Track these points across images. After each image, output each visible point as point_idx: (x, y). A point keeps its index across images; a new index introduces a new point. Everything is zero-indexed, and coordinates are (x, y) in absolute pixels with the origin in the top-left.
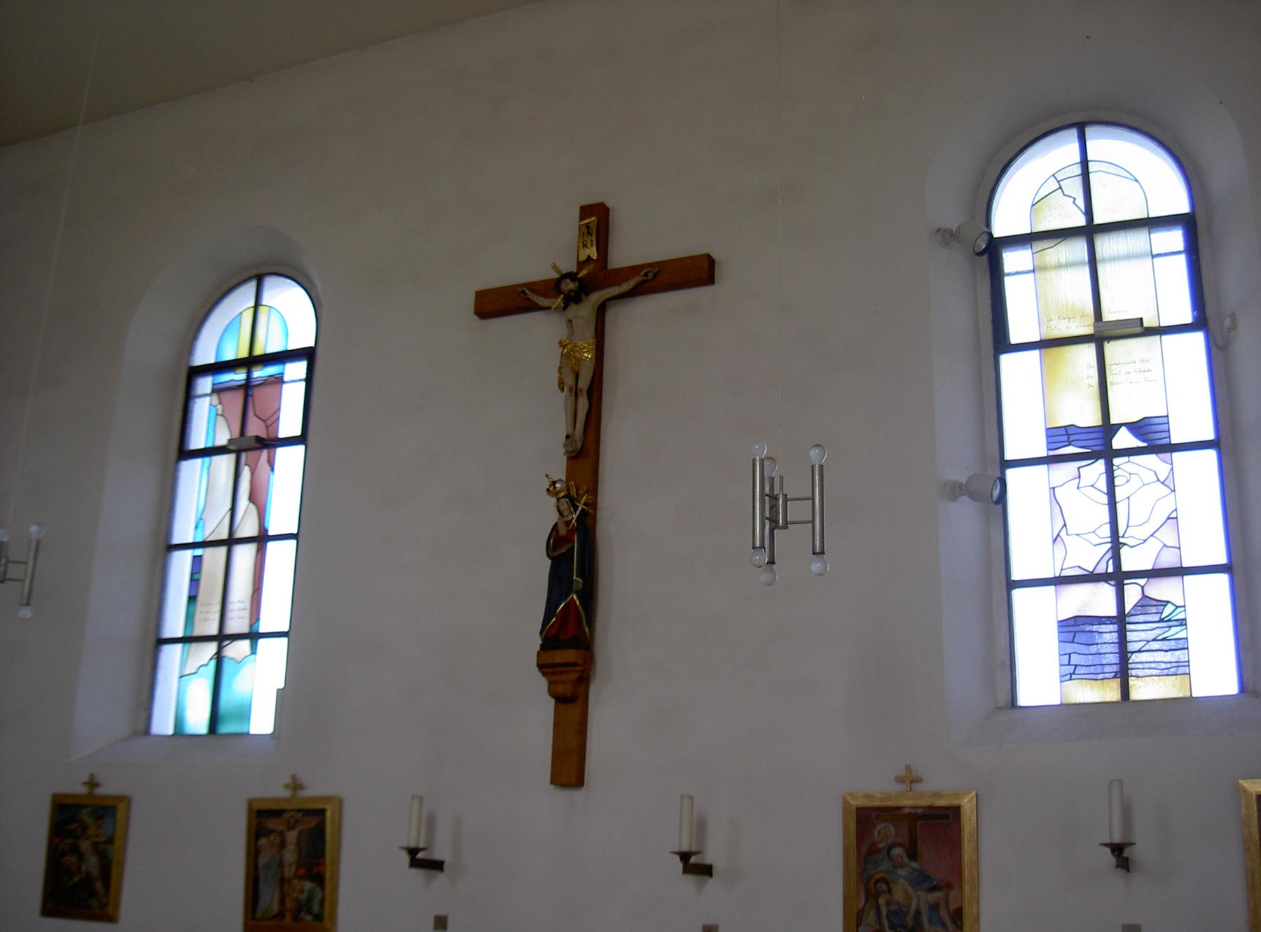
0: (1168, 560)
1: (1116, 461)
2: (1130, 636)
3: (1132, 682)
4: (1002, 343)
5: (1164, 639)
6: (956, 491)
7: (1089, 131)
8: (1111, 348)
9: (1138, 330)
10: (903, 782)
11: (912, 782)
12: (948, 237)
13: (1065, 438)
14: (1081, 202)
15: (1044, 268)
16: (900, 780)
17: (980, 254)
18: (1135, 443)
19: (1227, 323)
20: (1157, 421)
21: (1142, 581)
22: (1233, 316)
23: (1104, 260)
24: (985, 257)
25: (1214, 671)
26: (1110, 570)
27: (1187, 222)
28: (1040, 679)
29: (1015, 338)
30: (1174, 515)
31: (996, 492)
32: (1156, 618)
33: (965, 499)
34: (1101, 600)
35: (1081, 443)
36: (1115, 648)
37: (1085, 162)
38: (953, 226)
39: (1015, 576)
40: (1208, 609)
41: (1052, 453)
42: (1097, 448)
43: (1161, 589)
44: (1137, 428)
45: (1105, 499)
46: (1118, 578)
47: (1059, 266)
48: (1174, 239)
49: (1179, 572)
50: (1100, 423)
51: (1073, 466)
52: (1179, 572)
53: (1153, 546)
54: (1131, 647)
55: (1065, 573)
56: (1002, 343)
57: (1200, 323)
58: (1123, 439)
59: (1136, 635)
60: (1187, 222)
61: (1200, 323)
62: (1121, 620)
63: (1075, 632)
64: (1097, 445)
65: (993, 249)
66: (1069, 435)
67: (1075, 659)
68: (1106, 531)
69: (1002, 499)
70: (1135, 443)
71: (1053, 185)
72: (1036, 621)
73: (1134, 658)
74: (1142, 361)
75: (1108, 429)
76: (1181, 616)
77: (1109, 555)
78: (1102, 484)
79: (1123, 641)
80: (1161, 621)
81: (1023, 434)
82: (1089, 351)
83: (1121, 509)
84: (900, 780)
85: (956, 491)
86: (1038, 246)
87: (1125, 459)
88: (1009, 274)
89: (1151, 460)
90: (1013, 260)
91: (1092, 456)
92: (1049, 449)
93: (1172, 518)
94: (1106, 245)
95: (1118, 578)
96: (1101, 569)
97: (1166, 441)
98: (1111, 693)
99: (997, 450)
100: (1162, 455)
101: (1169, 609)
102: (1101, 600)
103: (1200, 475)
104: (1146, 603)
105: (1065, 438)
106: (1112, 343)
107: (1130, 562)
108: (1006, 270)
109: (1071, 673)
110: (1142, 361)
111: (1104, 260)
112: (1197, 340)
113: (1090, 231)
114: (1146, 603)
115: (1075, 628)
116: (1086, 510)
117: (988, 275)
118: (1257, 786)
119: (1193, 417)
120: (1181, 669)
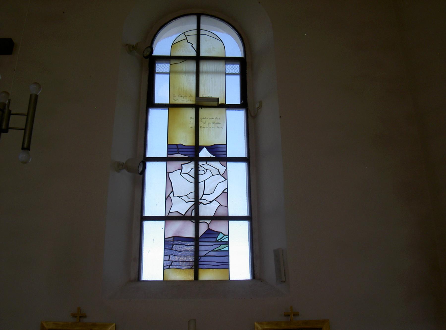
0: (222, 212)
1: (200, 163)
2: (201, 248)
3: (200, 271)
4: (151, 103)
5: (217, 251)
6: (120, 167)
7: (203, 19)
8: (203, 112)
9: (215, 104)
10: (76, 317)
11: (80, 317)
12: (131, 48)
13: (176, 150)
14: (195, 46)
15: (176, 72)
16: (74, 316)
17: (146, 58)
18: (209, 155)
19: (257, 105)
20: (221, 146)
21: (208, 222)
22: (261, 102)
23: (203, 72)
24: (148, 59)
25: (240, 268)
26: (193, 215)
27: (242, 62)
28: (153, 268)
29: (158, 100)
30: (226, 191)
31: (141, 169)
32: (214, 240)
33: (125, 171)
34: (188, 230)
35: (184, 153)
36: (193, 253)
37: (199, 29)
38: (134, 43)
39: (147, 213)
40: (239, 237)
41: (169, 156)
42: (191, 156)
43: (217, 226)
44: (210, 149)
45: (193, 180)
46: (196, 219)
47: (182, 72)
48: (236, 68)
49: (228, 218)
50: (194, 145)
51: (179, 163)
52: (228, 218)
53: (215, 205)
54: (202, 254)
55: (170, 215)
56: (151, 103)
57: (243, 105)
58: (204, 153)
59: (204, 248)
60: (242, 62)
61: (243, 105)
62: (196, 240)
63: (173, 245)
64: (191, 154)
65: (153, 60)
66: (178, 149)
67: (172, 258)
68: (192, 196)
69: (143, 173)
70: (209, 155)
71: (183, 37)
72: (154, 237)
73: (203, 259)
74: (216, 118)
75: (197, 148)
76: (227, 240)
77: (193, 207)
78: (193, 173)
79: (197, 251)
80: (217, 241)
81: (156, 145)
82: (191, 112)
83: (201, 185)
84: (74, 316)
85: (120, 167)
86: (173, 62)
87: (205, 163)
88: (158, 73)
89: (217, 164)
90: (160, 67)
91: (189, 160)
92: (167, 154)
93: (225, 192)
94: (204, 66)
95: (196, 219)
96: (189, 214)
97: (225, 156)
98: (190, 276)
99: (142, 152)
100: (222, 162)
101: (220, 236)
102: (188, 230)
103: (238, 173)
104: (210, 233)
105: (176, 150)
106: (203, 109)
107: (204, 211)
108: (157, 71)
109: (168, 265)
110: (216, 118)
111: (203, 72)
112: (241, 115)
113: (198, 59)
114: (210, 233)
115: (170, 243)
116: (183, 184)
117: (148, 72)
118: (324, 328)
119: (237, 146)
120: (226, 266)
